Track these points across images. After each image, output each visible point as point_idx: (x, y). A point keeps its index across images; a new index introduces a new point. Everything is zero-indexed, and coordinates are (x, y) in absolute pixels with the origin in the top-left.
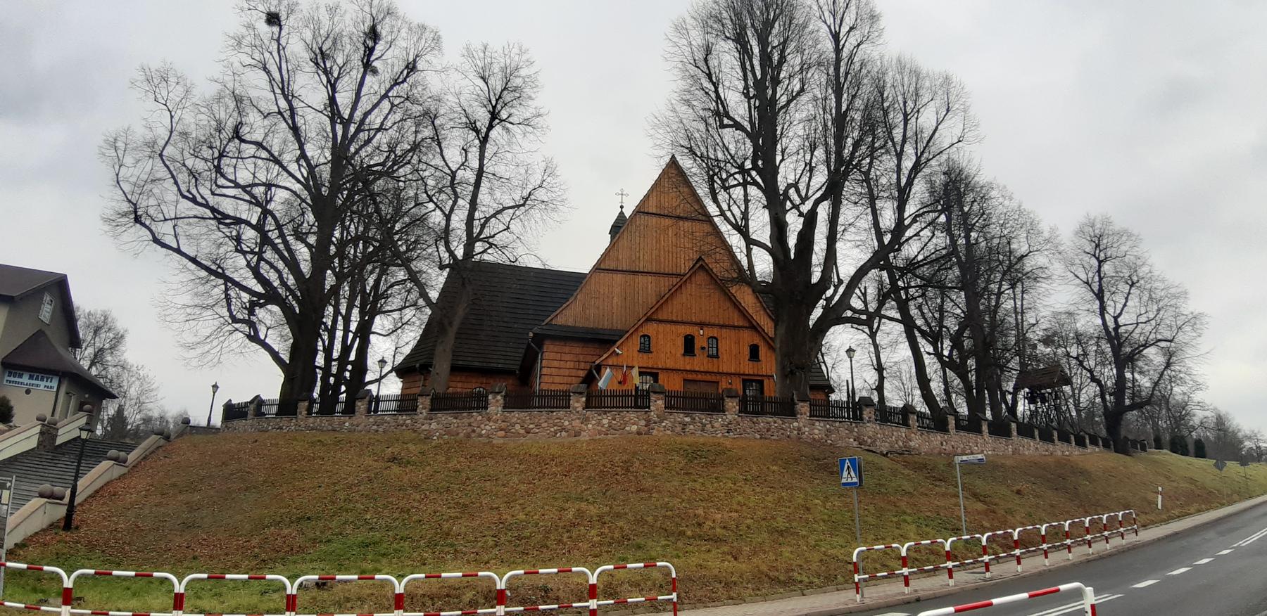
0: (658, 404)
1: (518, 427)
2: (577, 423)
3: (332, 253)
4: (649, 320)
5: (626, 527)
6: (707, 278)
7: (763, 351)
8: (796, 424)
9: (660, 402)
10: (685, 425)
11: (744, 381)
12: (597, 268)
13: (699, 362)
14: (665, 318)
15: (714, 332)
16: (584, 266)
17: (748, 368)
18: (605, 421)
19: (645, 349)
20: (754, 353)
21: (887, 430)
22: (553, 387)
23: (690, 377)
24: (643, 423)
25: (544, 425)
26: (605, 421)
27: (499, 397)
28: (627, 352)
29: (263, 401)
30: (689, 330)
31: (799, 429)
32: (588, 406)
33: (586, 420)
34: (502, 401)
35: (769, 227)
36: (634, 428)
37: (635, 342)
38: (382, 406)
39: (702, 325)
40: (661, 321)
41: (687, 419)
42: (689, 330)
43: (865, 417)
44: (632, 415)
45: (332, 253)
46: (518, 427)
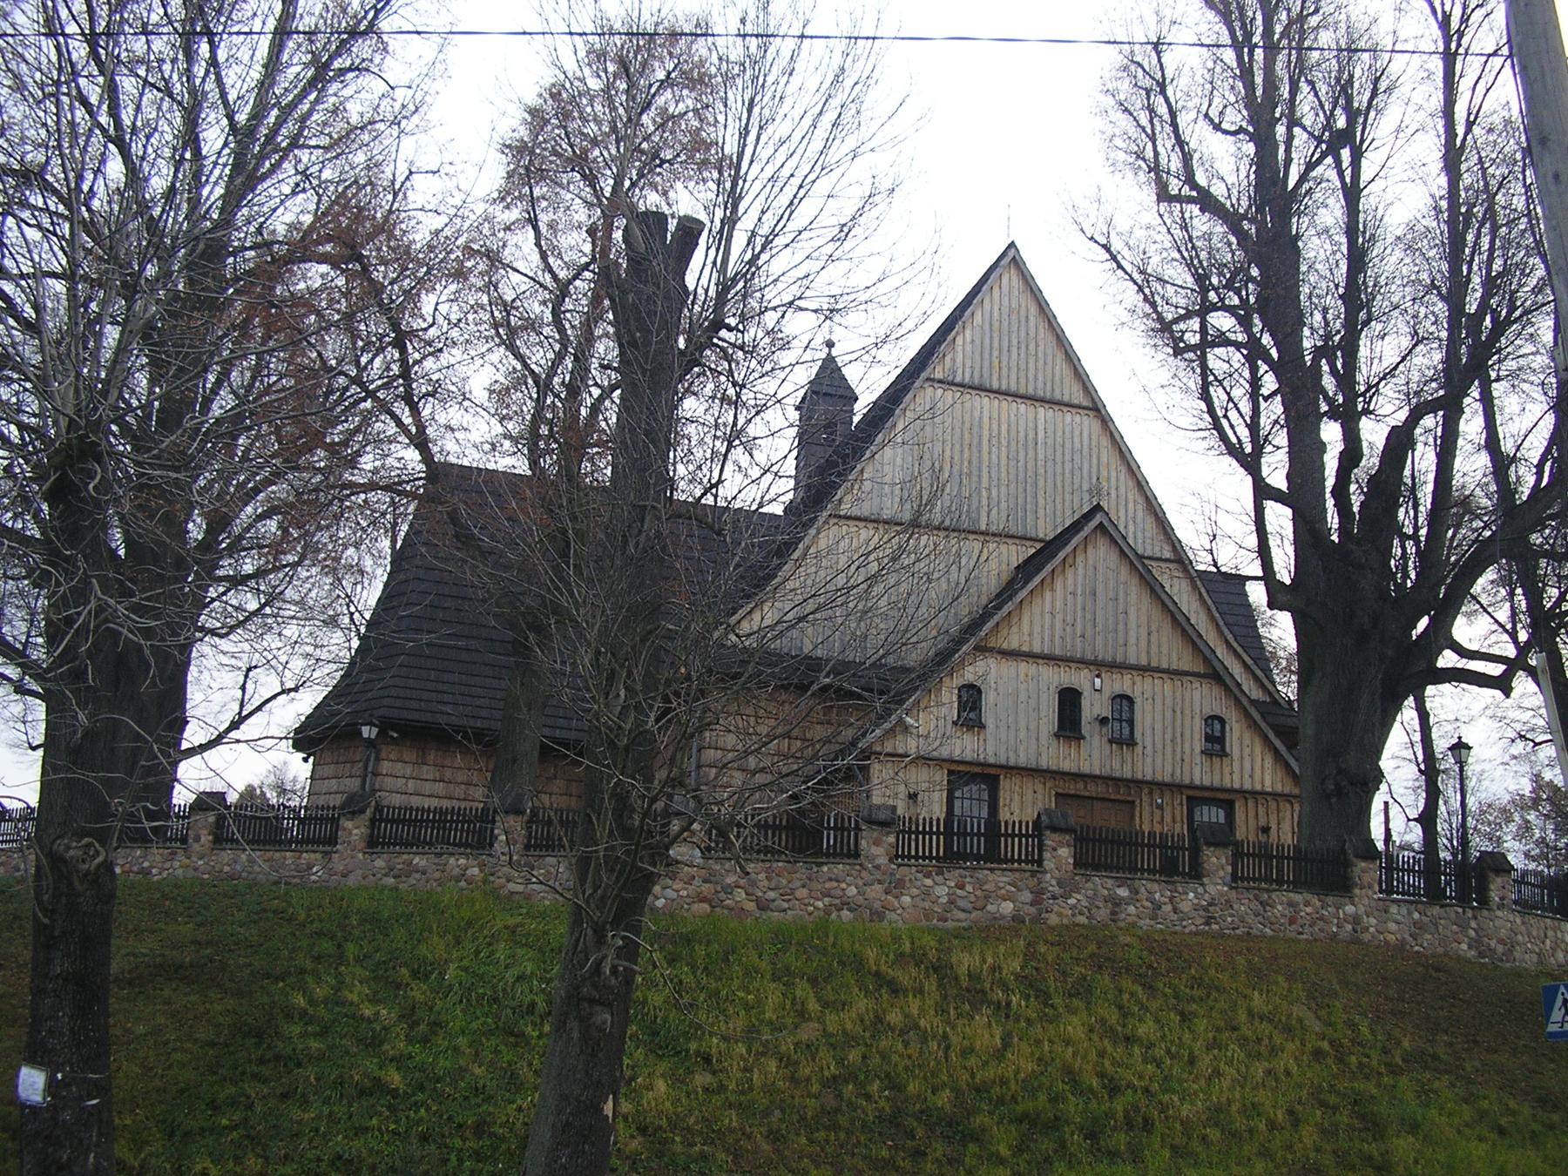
1: (740, 895)
2: (876, 891)
5: (297, 1114)
6: (1114, 557)
7: (1238, 735)
8: (1350, 909)
9: (1065, 852)
10: (1117, 903)
11: (950, 773)
13: (1093, 755)
14: (1014, 645)
15: (1122, 683)
17: (1200, 773)
18: (941, 891)
20: (1215, 744)
23: (1071, 788)
24: (1027, 896)
25: (802, 893)
26: (941, 891)
28: (931, 723)
31: (1356, 920)
36: (1007, 908)
37: (948, 699)
39: (1099, 666)
41: (1123, 892)
43: (1495, 896)
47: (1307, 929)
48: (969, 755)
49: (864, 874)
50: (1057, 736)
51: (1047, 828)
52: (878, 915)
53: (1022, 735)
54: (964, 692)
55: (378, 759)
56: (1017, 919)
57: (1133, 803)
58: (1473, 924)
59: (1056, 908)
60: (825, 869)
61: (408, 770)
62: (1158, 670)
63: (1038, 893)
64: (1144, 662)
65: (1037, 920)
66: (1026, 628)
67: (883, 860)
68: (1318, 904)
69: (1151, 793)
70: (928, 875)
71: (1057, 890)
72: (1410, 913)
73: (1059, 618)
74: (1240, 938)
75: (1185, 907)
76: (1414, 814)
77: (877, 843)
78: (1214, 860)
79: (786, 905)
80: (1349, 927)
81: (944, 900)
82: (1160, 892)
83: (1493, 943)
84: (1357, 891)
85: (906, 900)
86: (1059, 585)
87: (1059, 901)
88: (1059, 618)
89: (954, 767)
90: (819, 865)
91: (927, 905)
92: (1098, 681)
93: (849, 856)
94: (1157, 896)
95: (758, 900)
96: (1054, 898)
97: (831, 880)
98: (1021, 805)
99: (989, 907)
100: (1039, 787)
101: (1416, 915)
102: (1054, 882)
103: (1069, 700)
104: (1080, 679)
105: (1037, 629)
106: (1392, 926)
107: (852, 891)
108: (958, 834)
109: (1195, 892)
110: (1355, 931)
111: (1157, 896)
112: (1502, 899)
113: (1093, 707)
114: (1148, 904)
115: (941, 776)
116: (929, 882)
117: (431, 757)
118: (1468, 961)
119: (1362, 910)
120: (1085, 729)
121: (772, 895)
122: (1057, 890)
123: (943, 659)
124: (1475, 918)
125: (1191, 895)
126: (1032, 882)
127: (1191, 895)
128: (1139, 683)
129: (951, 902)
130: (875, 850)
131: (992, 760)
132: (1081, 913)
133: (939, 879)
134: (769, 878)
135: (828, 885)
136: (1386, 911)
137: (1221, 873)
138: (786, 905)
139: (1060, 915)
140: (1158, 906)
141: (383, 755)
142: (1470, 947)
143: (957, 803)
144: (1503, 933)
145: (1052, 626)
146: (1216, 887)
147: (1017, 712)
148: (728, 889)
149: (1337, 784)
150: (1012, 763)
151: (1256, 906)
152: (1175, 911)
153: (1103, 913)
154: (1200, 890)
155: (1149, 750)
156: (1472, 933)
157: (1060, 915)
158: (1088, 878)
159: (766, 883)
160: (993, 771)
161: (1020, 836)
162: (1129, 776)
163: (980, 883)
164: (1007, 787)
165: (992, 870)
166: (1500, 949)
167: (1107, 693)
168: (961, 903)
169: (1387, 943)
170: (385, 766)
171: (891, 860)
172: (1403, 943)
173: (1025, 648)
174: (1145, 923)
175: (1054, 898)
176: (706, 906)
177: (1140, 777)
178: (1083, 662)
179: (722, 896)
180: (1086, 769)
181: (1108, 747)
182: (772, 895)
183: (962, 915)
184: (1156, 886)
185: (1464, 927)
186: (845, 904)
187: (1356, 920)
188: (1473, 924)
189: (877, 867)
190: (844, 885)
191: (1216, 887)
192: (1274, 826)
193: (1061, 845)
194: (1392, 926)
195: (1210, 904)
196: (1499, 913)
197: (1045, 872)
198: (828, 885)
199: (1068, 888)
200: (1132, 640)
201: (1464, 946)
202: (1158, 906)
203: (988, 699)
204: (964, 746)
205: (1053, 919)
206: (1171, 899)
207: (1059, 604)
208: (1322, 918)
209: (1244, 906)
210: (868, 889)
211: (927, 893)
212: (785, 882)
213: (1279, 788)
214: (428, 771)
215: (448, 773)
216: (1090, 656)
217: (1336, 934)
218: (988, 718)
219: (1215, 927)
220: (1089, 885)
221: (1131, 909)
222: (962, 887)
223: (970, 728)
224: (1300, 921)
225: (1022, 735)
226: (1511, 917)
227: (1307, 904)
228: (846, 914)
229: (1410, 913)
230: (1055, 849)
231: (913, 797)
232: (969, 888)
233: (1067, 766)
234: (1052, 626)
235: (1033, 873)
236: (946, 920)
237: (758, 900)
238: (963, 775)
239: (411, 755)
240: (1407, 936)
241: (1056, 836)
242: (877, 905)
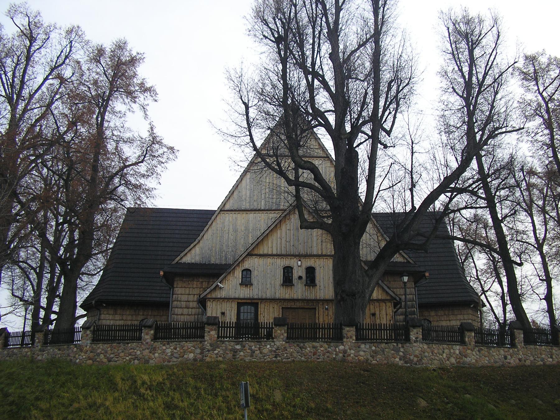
0: (211, 334)
1: (102, 356)
2: (146, 352)
3: (451, 186)
4: (250, 255)
8: (341, 347)
9: (213, 333)
10: (235, 352)
12: (222, 209)
13: (299, 291)
15: (310, 262)
16: (214, 206)
18: (169, 351)
19: (246, 281)
21: (436, 348)
22: (460, 299)
23: (286, 305)
24: (198, 351)
27: (88, 332)
28: (231, 286)
29: (9, 333)
30: (287, 262)
31: (345, 352)
32: (155, 338)
33: (153, 350)
34: (90, 335)
35: (378, 157)
36: (191, 356)
38: (12, 341)
39: (300, 256)
40: (261, 256)
41: (238, 347)
42: (287, 262)
43: (413, 337)
44: (189, 345)
45: (451, 186)
46: (102, 356)
47: (322, 357)
48: (247, 296)
49: (142, 346)
50: (283, 285)
51: (206, 324)
52: (147, 362)
53: (268, 286)
54: (245, 273)
55: (100, 314)
56: (195, 360)
57: (315, 309)
58: (402, 350)
59: (209, 355)
60: (130, 345)
61: (111, 317)
62: (325, 256)
63: (202, 349)
64: (320, 253)
65: (202, 360)
66: (270, 245)
67: (149, 340)
68: (327, 346)
69: (323, 304)
70: (164, 345)
71: (209, 348)
72: (370, 347)
73: (283, 240)
74: (290, 362)
75: (265, 351)
76: (543, 297)
77: (147, 334)
78: (279, 331)
79: (116, 359)
80: (341, 355)
81: (169, 354)
82: (254, 346)
83: (412, 357)
84: (345, 340)
85: (157, 355)
86: (283, 227)
87: (211, 352)
88: (283, 240)
89: (240, 301)
90: (128, 343)
91: (163, 356)
92: (299, 263)
93: (137, 340)
94: (253, 347)
95: (108, 358)
96: (209, 351)
97: (131, 349)
98: (267, 315)
99: (185, 356)
100: (276, 306)
101: (374, 348)
102: (208, 345)
103: (288, 271)
104: (293, 262)
105: (274, 245)
106: (362, 353)
107: (139, 353)
108: (222, 327)
109: (270, 345)
110: (344, 356)
111: (253, 347)
112: (416, 338)
113: (299, 271)
114: (249, 351)
115: (235, 306)
116: (164, 348)
117: (119, 312)
118: (401, 367)
119: (347, 347)
120: (295, 281)
121: (112, 356)
122: (209, 348)
123: (238, 262)
124: (403, 347)
125: (268, 346)
126: (200, 345)
127: (268, 346)
128: (317, 262)
129: (172, 355)
130: (147, 337)
131: (255, 297)
132: (220, 356)
133: (168, 346)
134: (111, 350)
135: (130, 351)
136: (359, 347)
137: (282, 337)
138: (116, 359)
139: (211, 357)
140: (253, 352)
141: (102, 312)
142: (400, 359)
143: (242, 315)
144: (417, 353)
145: (281, 243)
146: (279, 343)
147: (266, 277)
148: (98, 355)
149: (341, 296)
150: (264, 297)
151: (298, 349)
152: (261, 353)
153: (230, 355)
154: (272, 344)
155: (322, 287)
156: (401, 354)
157: (211, 357)
158: (223, 342)
159: (110, 352)
160: (256, 301)
161: (230, 327)
162: (313, 298)
163: (182, 347)
164: (262, 308)
165: (186, 342)
166: (416, 359)
167: (304, 266)
168: (175, 355)
169: (359, 360)
170: (103, 316)
171: (152, 340)
172: (367, 360)
173: (270, 253)
174: (247, 359)
175: (209, 351)
176: (91, 361)
177: (318, 298)
178: (294, 256)
179: (96, 357)
180: (295, 297)
181: (304, 287)
182: (112, 356)
183: (175, 360)
184: (253, 344)
185: (398, 351)
186: (136, 358)
187: (345, 352)
188: (402, 350)
189: (147, 343)
190: (136, 351)
191: (279, 343)
192: (377, 313)
193: (212, 330)
194: (362, 353)
195: (277, 350)
196: (415, 344)
197: (205, 341)
198: (130, 351)
199: (214, 347)
200: (315, 245)
201: (397, 359)
202: (253, 352)
203: (255, 274)
204: (245, 293)
205: (208, 359)
206: (259, 349)
207: (284, 234)
208: (328, 352)
209: (293, 349)
210: (144, 351)
211: (164, 352)
212: (116, 351)
213: (380, 297)
214: (117, 317)
215: (124, 318)
216: (297, 253)
217: (334, 359)
218: (254, 281)
219: (278, 358)
220: (223, 345)
221: (242, 353)
222: (176, 349)
223: (246, 285)
224: (318, 354)
225: (268, 286)
226: (421, 346)
227: (321, 346)
228: (136, 361)
229: (370, 347)
230: (209, 332)
231: (223, 314)
232: (178, 349)
233: (287, 297)
234: (281, 243)
235: (201, 342)
236: (170, 362)
237: (108, 358)
238: (241, 303)
239: (111, 312)
240: (369, 357)
241: (210, 327)
242: (147, 357)
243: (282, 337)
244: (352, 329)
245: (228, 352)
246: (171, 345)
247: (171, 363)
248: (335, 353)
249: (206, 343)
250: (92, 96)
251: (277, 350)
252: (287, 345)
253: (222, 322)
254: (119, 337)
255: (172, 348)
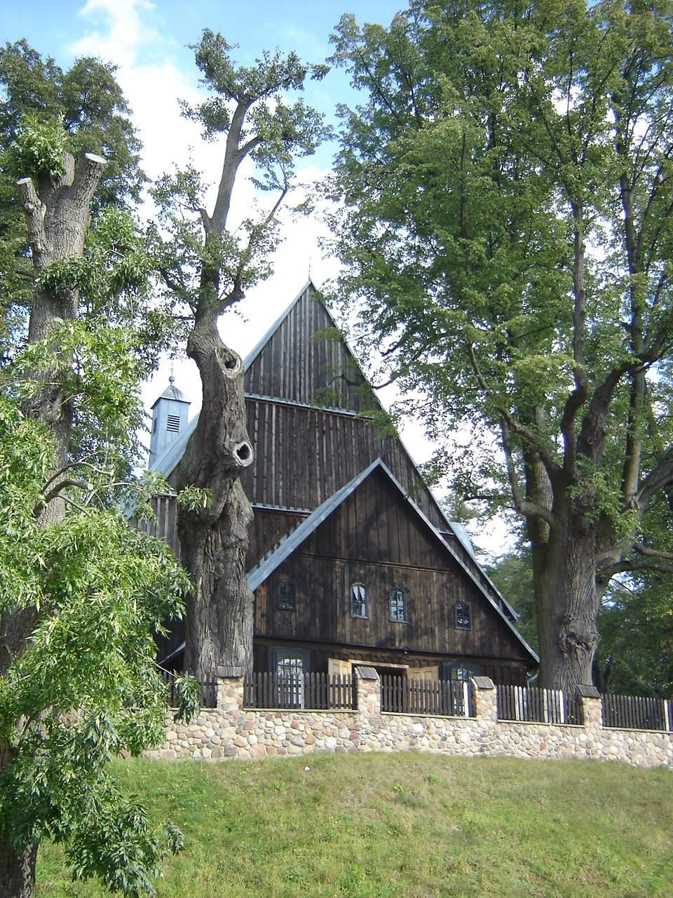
2: (229, 733)
8: (583, 737)
24: (346, 733)
31: (588, 746)
33: (243, 728)
63: (354, 730)
67: (234, 708)
71: (370, 728)
77: (230, 694)
84: (587, 723)
85: (253, 739)
87: (371, 735)
102: (366, 721)
107: (211, 733)
116: (270, 724)
119: (591, 738)
126: (350, 721)
130: (228, 700)
133: (278, 721)
195: (482, 736)
230: (366, 696)
243: (490, 712)
244: (596, 704)
245: (402, 738)
246: (285, 718)
247: (285, 756)
248: (573, 746)
249: (362, 716)
250: (641, 91)
251: (482, 736)
252: (499, 727)
253: (334, 677)
254: (297, 694)
255: (288, 724)
